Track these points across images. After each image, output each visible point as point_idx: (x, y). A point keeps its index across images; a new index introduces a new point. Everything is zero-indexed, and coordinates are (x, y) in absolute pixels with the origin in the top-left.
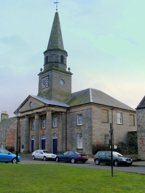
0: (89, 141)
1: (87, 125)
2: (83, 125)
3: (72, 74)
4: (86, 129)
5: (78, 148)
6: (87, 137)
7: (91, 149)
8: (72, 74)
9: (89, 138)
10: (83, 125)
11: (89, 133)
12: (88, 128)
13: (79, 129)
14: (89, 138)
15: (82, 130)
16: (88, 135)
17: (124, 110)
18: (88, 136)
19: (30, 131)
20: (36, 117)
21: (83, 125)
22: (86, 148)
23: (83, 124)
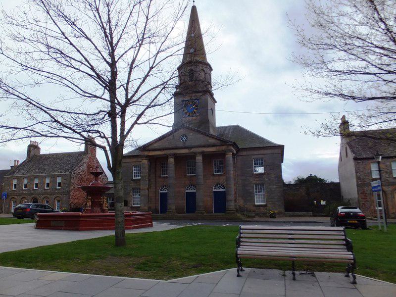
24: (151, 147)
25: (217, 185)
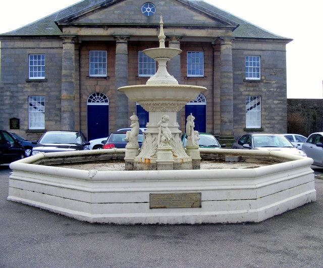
0: (280, 114)
1: (274, 82)
2: (265, 81)
3: (287, 41)
4: (272, 89)
5: (248, 127)
6: (273, 106)
7: (285, 124)
8: (287, 41)
9: (279, 108)
10: (45, 81)
11: (279, 98)
12: (277, 88)
13: (252, 89)
14: (279, 108)
15: (261, 91)
16: (276, 102)
17: (283, 87)
18: (276, 104)
19: (83, 78)
20: (122, 48)
21: (265, 81)
22: (272, 127)
23: (263, 78)
24: (82, 21)
25: (94, 95)
